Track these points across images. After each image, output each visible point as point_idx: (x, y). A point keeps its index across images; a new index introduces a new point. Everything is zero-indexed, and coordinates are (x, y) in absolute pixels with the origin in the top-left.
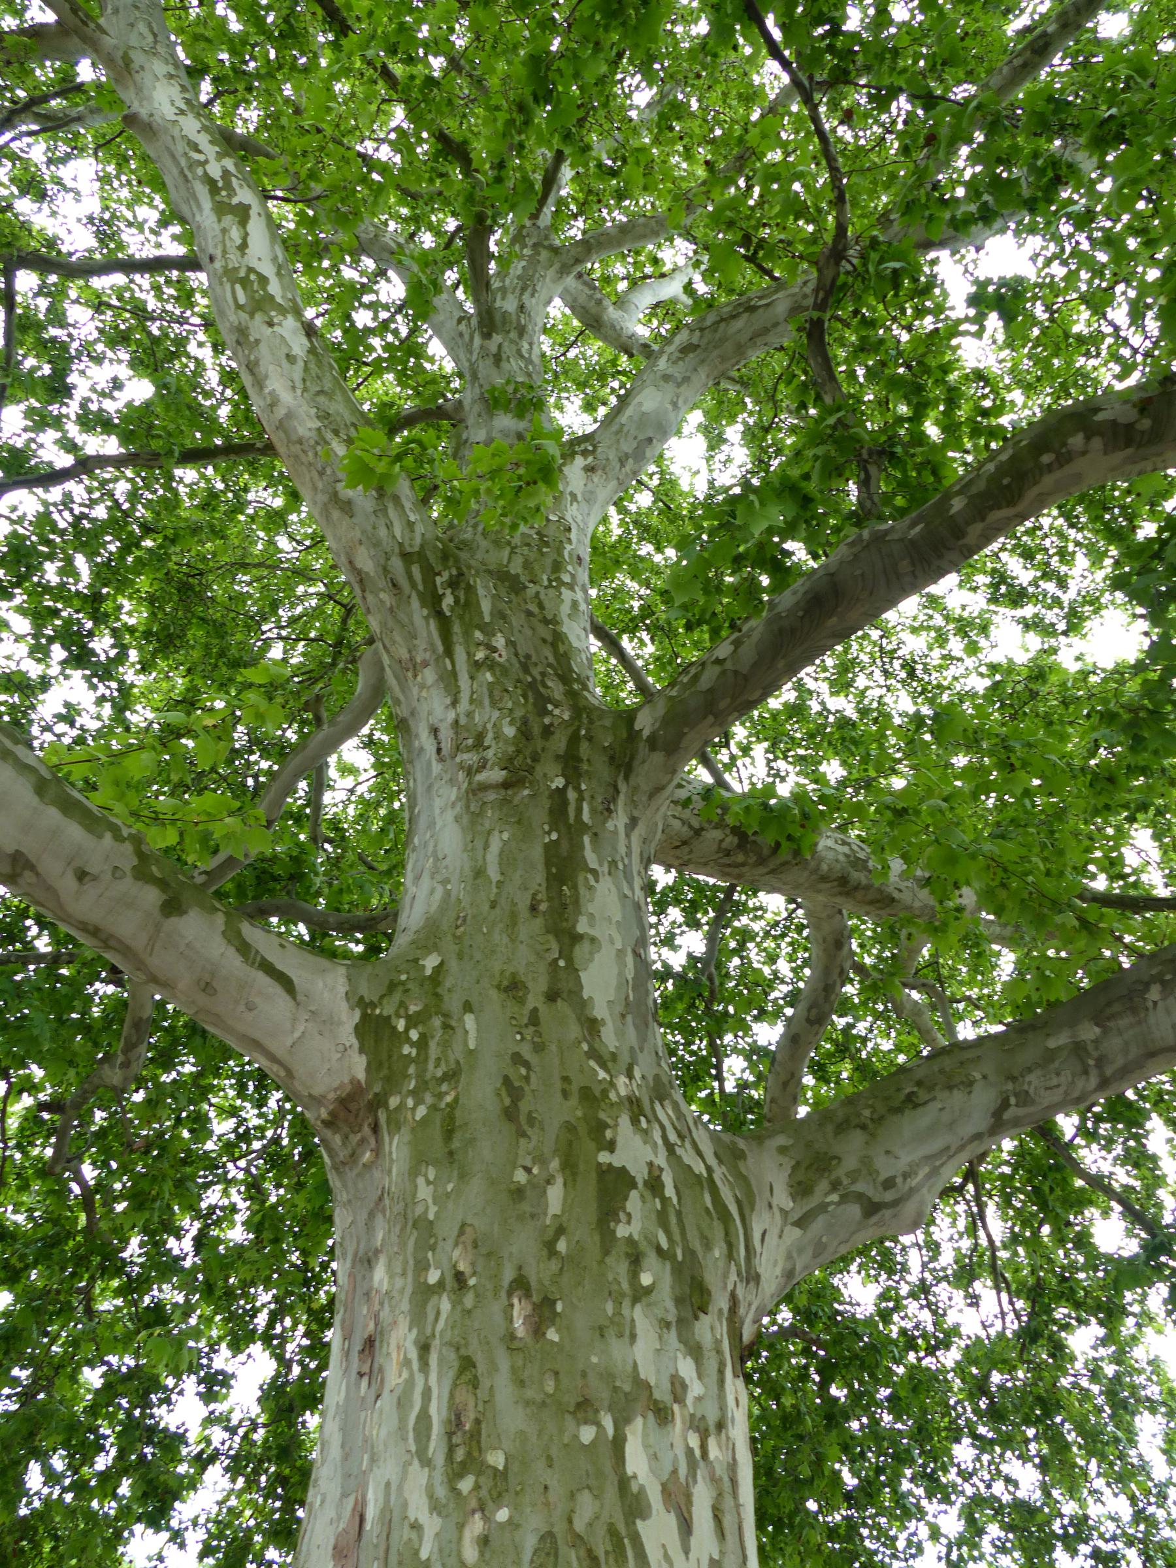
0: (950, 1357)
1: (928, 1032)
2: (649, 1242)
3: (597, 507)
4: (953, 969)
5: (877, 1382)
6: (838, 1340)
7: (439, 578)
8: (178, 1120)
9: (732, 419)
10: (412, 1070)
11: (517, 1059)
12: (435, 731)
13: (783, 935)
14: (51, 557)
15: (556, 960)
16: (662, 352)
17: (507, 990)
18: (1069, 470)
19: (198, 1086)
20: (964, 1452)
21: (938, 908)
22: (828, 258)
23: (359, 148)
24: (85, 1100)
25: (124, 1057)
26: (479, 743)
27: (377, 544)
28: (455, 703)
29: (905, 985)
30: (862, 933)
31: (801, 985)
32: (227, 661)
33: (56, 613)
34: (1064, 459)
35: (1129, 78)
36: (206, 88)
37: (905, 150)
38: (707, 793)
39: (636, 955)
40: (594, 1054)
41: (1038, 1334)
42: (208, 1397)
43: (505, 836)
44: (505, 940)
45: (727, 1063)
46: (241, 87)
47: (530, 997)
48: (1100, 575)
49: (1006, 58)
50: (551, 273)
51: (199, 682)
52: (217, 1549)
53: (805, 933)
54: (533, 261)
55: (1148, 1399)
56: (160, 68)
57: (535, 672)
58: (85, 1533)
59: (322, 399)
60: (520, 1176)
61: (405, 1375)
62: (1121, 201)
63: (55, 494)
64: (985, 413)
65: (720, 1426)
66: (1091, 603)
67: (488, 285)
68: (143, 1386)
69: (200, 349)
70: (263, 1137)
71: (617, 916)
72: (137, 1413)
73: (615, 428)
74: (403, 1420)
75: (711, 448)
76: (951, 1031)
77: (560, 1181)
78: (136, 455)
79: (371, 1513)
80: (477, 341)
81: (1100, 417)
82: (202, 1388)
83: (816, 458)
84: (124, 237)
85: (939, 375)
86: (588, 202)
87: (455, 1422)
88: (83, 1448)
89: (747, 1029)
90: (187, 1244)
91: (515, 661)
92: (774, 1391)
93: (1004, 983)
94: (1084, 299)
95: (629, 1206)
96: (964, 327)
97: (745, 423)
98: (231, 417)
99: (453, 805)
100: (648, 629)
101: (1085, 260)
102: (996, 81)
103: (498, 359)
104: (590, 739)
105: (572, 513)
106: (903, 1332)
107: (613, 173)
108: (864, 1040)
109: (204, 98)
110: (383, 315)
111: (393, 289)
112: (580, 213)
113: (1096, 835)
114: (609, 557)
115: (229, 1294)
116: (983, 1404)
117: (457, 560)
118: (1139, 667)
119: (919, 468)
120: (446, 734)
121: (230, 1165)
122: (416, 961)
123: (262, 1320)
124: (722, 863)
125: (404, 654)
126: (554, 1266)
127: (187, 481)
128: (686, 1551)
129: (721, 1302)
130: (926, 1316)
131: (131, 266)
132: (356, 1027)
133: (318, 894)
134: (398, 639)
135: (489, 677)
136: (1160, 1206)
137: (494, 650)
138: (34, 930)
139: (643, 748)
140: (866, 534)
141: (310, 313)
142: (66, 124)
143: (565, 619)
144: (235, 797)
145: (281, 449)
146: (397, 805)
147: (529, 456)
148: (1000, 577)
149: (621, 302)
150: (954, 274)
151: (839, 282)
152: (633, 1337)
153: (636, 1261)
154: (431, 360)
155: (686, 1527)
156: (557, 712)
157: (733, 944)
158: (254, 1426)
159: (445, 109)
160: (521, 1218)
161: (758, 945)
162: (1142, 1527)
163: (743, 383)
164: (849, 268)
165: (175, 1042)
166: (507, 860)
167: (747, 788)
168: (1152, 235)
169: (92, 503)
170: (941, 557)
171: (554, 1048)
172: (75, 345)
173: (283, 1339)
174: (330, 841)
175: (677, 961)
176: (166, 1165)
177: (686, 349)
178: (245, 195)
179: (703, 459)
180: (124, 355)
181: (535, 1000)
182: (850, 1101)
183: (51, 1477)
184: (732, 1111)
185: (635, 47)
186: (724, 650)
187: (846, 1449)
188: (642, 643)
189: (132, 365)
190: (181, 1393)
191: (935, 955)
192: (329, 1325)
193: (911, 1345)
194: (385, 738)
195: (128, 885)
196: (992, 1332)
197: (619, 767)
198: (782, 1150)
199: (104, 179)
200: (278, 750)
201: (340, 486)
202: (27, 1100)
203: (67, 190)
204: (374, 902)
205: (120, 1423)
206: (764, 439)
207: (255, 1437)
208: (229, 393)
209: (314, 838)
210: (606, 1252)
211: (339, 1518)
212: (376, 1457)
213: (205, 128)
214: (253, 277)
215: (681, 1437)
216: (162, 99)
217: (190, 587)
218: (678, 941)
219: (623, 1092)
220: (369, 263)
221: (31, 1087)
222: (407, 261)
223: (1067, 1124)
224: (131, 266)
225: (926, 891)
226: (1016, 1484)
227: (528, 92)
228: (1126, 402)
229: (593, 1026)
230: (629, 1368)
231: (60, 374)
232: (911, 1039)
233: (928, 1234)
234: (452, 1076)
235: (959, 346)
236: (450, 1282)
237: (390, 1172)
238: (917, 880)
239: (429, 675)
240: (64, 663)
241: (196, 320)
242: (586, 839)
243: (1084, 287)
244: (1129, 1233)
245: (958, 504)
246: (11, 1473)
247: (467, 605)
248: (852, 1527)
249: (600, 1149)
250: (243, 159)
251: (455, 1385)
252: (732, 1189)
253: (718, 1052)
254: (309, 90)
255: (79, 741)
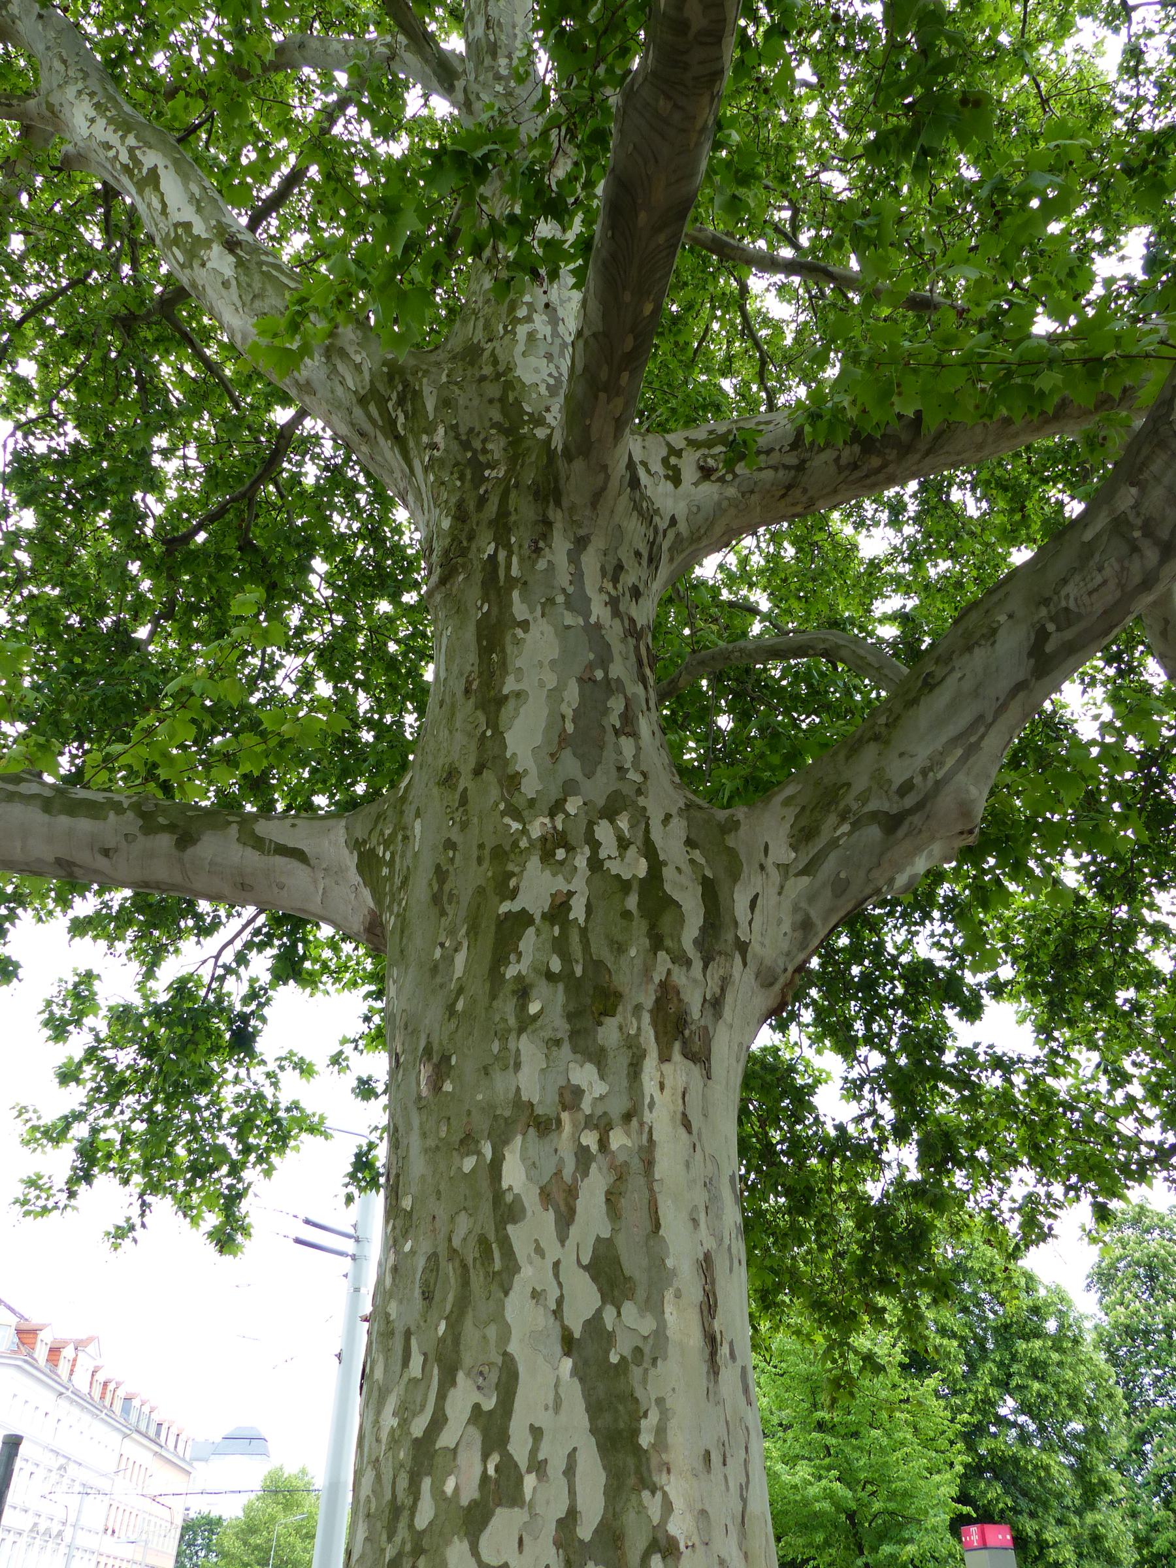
59: (258, 304)
95: (522, 946)
123: (859, 1026)
139: (561, 464)
143: (519, 360)
152: (517, 1066)
153: (523, 993)
195: (142, 842)
210: (493, 997)
230: (511, 1095)
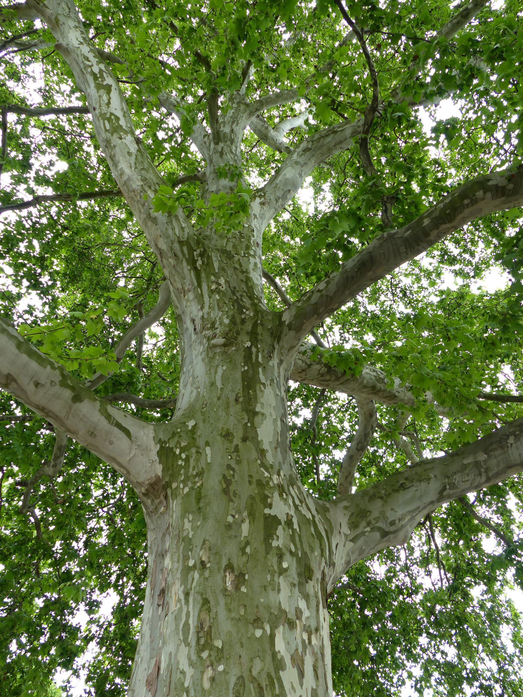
0: (418, 598)
1: (410, 454)
2: (287, 549)
3: (266, 220)
4: (421, 426)
5: (386, 609)
6: (368, 590)
7: (196, 252)
8: (77, 490)
9: (326, 180)
10: (182, 471)
11: (229, 467)
12: (193, 321)
13: (346, 411)
14: (22, 240)
15: (246, 423)
16: (295, 151)
17: (225, 436)
18: (476, 207)
19: (86, 475)
20: (423, 640)
21: (415, 400)
22: (369, 111)
23: (160, 58)
24: (37, 481)
25: (54, 461)
26: (213, 326)
27: (168, 237)
28: (202, 308)
29: (400, 434)
30: (381, 410)
31: (354, 433)
32: (101, 287)
33: (24, 265)
34: (474, 202)
35: (505, 30)
36: (92, 32)
37: (404, 62)
38: (314, 348)
39: (282, 421)
40: (263, 465)
41: (457, 589)
42: (90, 612)
43: (224, 368)
44: (224, 414)
45: (321, 467)
46: (107, 31)
47: (235, 440)
48: (489, 251)
49: (449, 19)
50: (245, 115)
51: (87, 296)
52: (93, 678)
53: (356, 410)
54: (237, 110)
55: (506, 618)
56: (72, 23)
57: (238, 295)
58: (35, 670)
59: (143, 172)
60: (230, 519)
61: (178, 606)
62: (500, 86)
63: (24, 212)
64: (439, 180)
65: (317, 630)
66: (485, 264)
67: (217, 120)
68: (62, 607)
69: (88, 148)
70: (115, 498)
71: (274, 404)
72: (59, 618)
73: (274, 185)
74: (177, 626)
75: (316, 193)
76: (420, 454)
77: (247, 521)
78: (60, 195)
79: (163, 666)
80: (212, 145)
81: (490, 183)
82: (87, 608)
83: (363, 200)
84: (55, 98)
85: (418, 163)
86: (262, 82)
87: (200, 627)
88: (35, 633)
89: (330, 452)
90: (81, 544)
91: (229, 290)
92: (340, 612)
93: (445, 433)
94: (484, 128)
95: (278, 533)
96: (430, 142)
97: (331, 182)
98: (103, 178)
99: (201, 354)
100: (287, 274)
101: (484, 110)
102: (445, 30)
103: (221, 154)
104: (262, 325)
105: (255, 223)
106: (397, 587)
107: (273, 71)
108: (382, 457)
109: (91, 36)
110: (170, 133)
111: (174, 121)
112: (259, 88)
113: (486, 367)
114: (271, 242)
115: (99, 567)
116: (432, 618)
117: (203, 244)
118: (507, 295)
119: (409, 205)
120: (198, 322)
121: (100, 510)
122: (185, 423)
123: (113, 578)
124: (321, 379)
125: (179, 286)
126: (245, 559)
127: (83, 207)
128: (302, 685)
129: (318, 575)
130: (407, 580)
131: (58, 111)
132: (158, 452)
133: (140, 391)
134: (177, 279)
135: (217, 297)
136: (512, 532)
137: (220, 285)
138: (14, 406)
139: (285, 329)
140: (385, 234)
141: (138, 132)
142: (29, 47)
143: (251, 271)
144: (104, 348)
145: (125, 194)
146: (175, 351)
147: (236, 200)
148: (445, 252)
149: (276, 127)
150: (426, 117)
151: (374, 121)
152: (279, 590)
153: (281, 557)
154: (192, 154)
155: (301, 674)
156: (247, 312)
157: (324, 415)
158: (110, 625)
159: (198, 42)
160: (230, 537)
161: (335, 415)
162: (502, 674)
163: (331, 164)
164: (379, 115)
165: (76, 455)
166: (225, 379)
167: (331, 346)
168: (515, 100)
169: (41, 217)
170: (418, 245)
171: (245, 462)
172: (33, 146)
173: (123, 585)
174: (146, 367)
175: (299, 422)
176: (72, 510)
177: (306, 150)
178: (109, 81)
179: (313, 199)
180: (55, 151)
181: (237, 441)
182: (376, 486)
183: (21, 646)
184: (324, 489)
185: (284, 15)
186: (322, 286)
187: (371, 638)
188: (285, 281)
189: (58, 155)
190: (78, 610)
191: (414, 420)
192: (143, 581)
193: (401, 592)
194: (170, 321)
195: (57, 388)
196: (437, 587)
197: (275, 337)
198: (346, 508)
199: (46, 72)
200: (124, 327)
201: (151, 211)
202: (11, 481)
203: (29, 77)
204: (165, 395)
205: (51, 622)
206: (340, 190)
207: (111, 629)
208: (101, 168)
209: (138, 366)
210: (268, 553)
211: (149, 668)
212: (164, 640)
213: (91, 50)
214: (113, 117)
215: (300, 635)
216: (73, 37)
217: (84, 254)
218: (300, 413)
219: (276, 482)
220: (164, 110)
221: (13, 475)
222: (181, 110)
223: (471, 496)
224: (58, 111)
225: (410, 393)
226: (446, 655)
227: (236, 35)
228: (502, 176)
229: (262, 453)
230: (277, 604)
231: (26, 158)
232: (402, 457)
233: (409, 544)
234: (200, 474)
235: (428, 150)
236: (198, 566)
237: (172, 516)
238: (406, 388)
239: (191, 296)
240: (28, 287)
241: (87, 135)
242: (260, 370)
243: (484, 122)
244: (499, 544)
245: (426, 222)
246: (4, 644)
247: (208, 264)
248: (373, 673)
249: (265, 507)
250: (109, 64)
251: (200, 611)
252: (323, 525)
253: (317, 462)
254: (138, 32)
255: (35, 322)
